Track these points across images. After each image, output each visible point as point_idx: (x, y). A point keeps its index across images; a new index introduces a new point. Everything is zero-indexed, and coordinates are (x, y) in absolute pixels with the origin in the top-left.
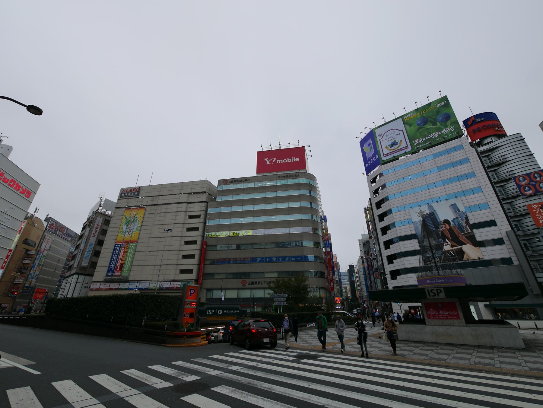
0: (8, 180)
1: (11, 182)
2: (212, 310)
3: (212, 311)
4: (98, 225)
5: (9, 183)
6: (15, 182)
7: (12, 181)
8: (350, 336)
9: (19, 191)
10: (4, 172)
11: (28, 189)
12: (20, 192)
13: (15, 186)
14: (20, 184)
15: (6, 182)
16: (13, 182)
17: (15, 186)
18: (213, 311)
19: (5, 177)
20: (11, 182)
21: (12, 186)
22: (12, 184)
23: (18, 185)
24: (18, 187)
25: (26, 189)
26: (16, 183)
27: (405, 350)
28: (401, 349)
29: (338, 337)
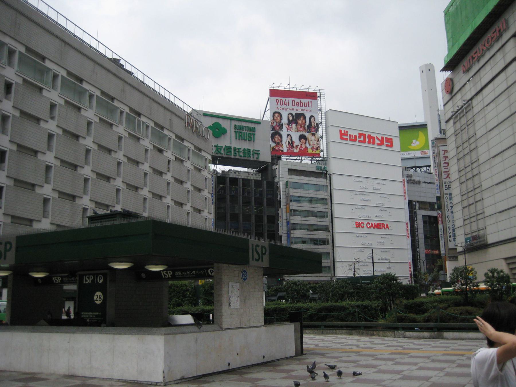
0: (355, 136)
1: (360, 137)
2: (90, 276)
3: (90, 278)
4: (445, 151)
5: (359, 140)
6: (364, 135)
7: (360, 135)
8: (333, 340)
9: (376, 144)
10: (346, 130)
11: (385, 137)
12: (378, 144)
13: (367, 140)
14: (372, 135)
15: (355, 140)
16: (362, 137)
17: (367, 140)
18: (91, 278)
19: (350, 135)
20: (360, 137)
21: (364, 142)
22: (362, 139)
23: (369, 136)
24: (371, 140)
25: (382, 138)
26: (367, 135)
27: (428, 369)
28: (433, 359)
29: (82, 210)
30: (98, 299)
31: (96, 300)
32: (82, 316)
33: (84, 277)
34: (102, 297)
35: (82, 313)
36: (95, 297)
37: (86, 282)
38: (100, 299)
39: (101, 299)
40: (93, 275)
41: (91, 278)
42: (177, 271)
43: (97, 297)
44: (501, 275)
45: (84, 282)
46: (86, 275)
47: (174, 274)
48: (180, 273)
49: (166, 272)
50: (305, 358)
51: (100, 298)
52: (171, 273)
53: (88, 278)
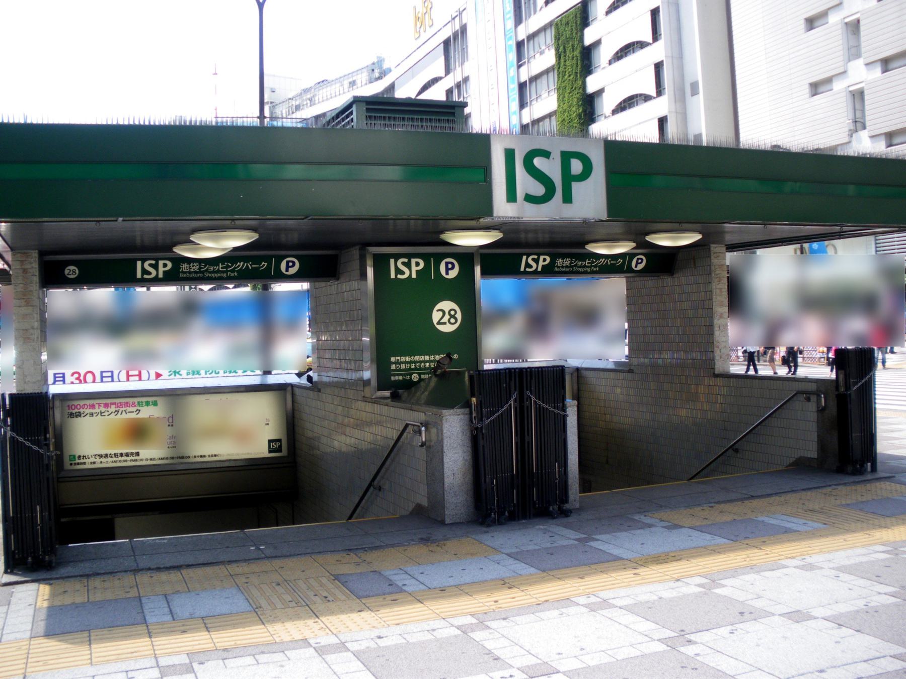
2: (413, 261)
18: (417, 264)
30: (445, 319)
31: (439, 323)
32: (393, 367)
33: (392, 261)
34: (459, 316)
35: (393, 359)
36: (436, 316)
37: (399, 276)
38: (453, 320)
39: (456, 321)
40: (425, 257)
41: (417, 265)
42: (564, 256)
43: (441, 314)
44: (725, 327)
45: (393, 276)
46: (397, 257)
47: (553, 262)
48: (567, 262)
49: (406, 260)
50: (616, 551)
51: (452, 316)
52: (422, 265)
53: (408, 265)
